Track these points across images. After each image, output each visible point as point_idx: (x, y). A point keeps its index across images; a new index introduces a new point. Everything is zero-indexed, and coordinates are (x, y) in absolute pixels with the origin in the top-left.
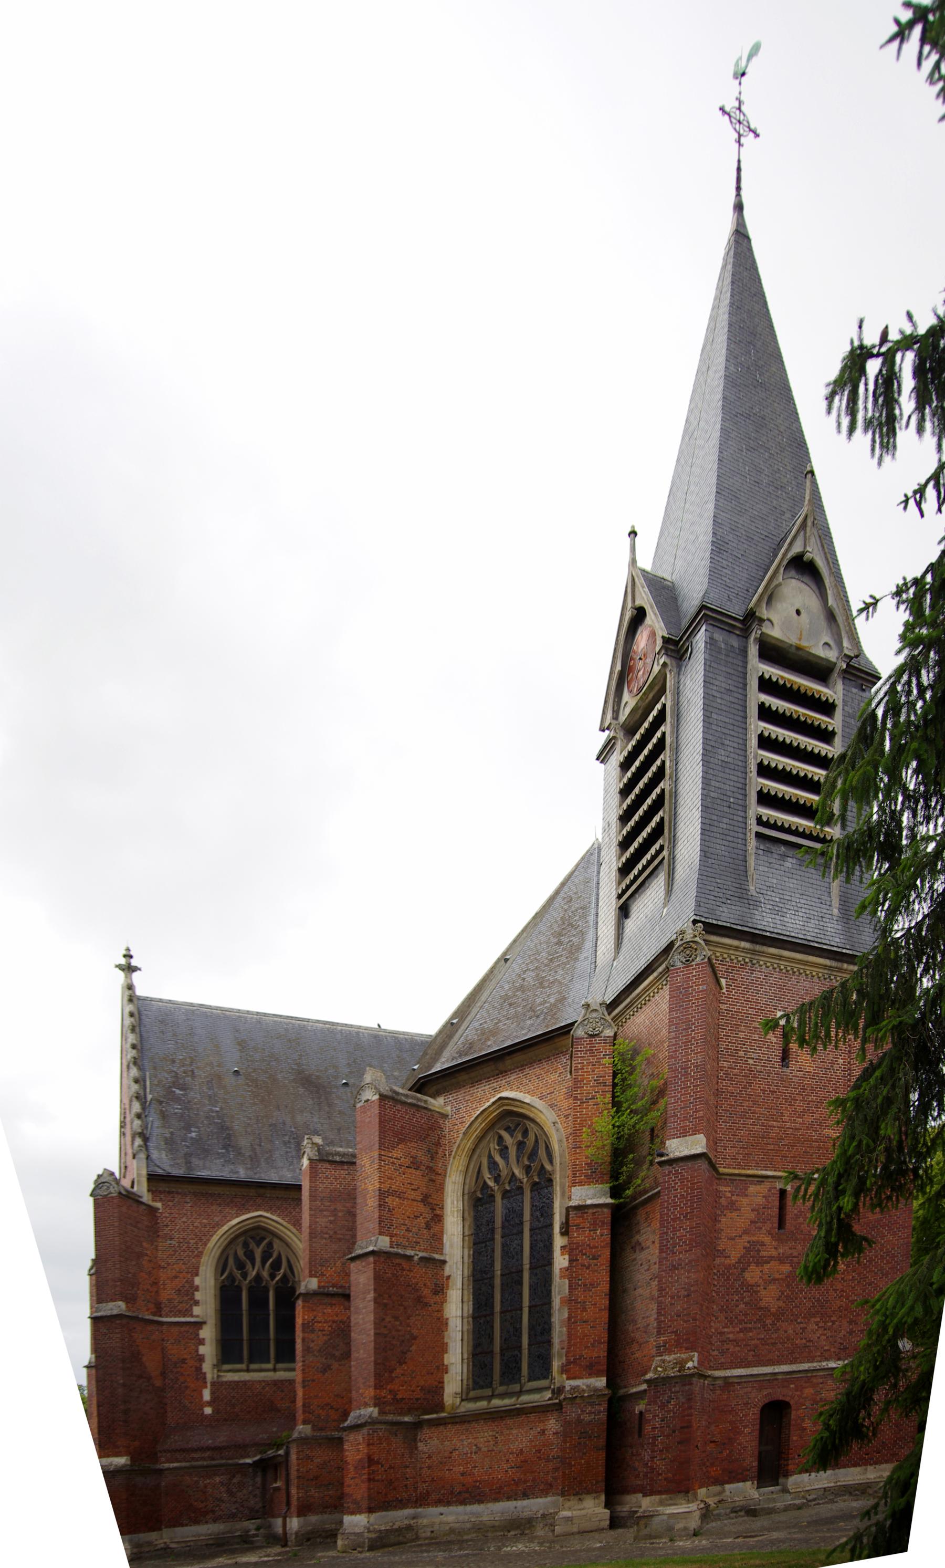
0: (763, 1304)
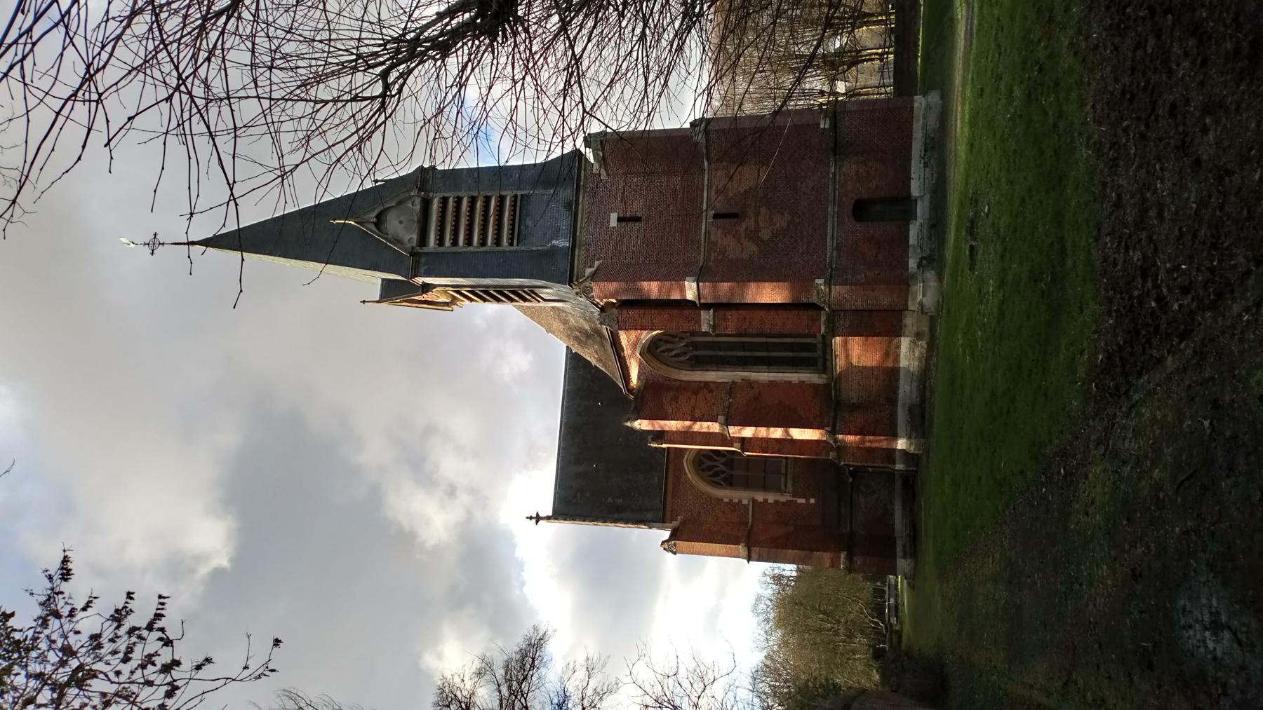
0: (785, 226)
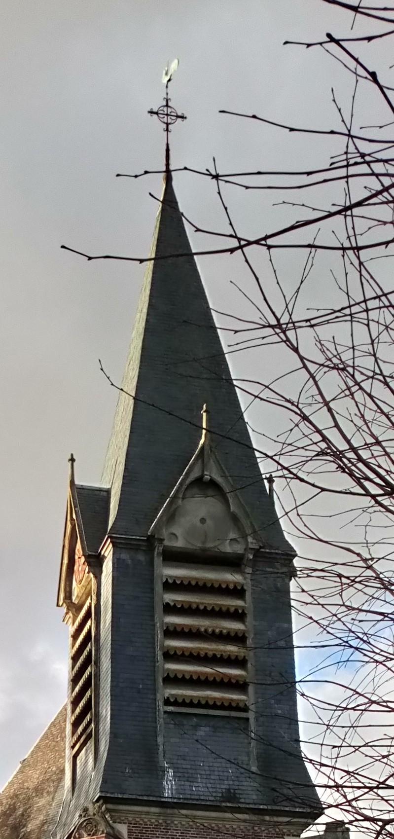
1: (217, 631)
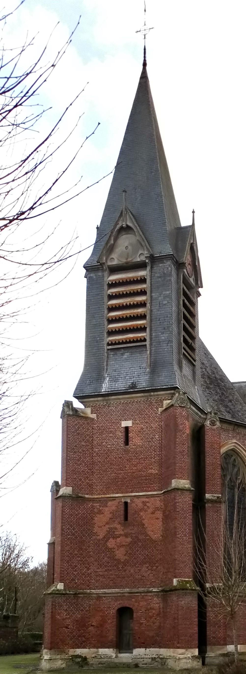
0: (117, 557)
1: (132, 303)
